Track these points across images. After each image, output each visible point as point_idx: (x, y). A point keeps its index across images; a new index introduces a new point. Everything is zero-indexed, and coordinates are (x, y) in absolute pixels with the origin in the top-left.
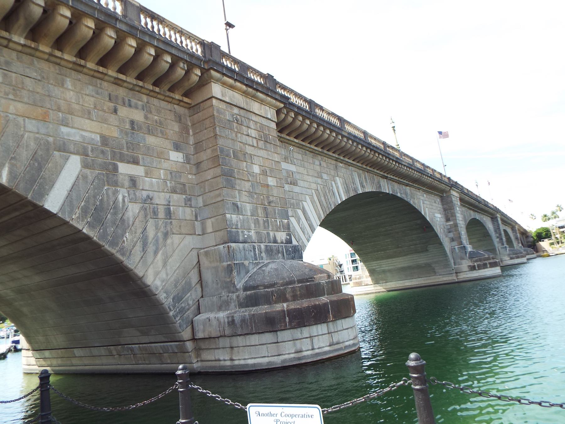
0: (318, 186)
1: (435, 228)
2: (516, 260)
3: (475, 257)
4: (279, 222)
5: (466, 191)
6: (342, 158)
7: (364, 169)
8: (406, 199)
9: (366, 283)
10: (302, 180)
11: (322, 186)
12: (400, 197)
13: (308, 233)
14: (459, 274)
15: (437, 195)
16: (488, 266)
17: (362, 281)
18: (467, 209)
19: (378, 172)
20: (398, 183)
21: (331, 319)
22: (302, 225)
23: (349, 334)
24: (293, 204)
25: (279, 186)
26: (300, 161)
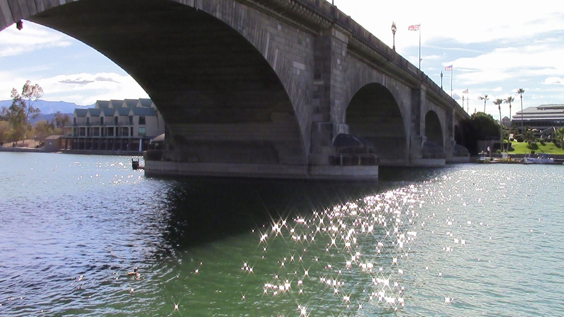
1: (285, 85)
8: (233, 25)
12: (221, 18)
15: (307, 31)
18: (365, 65)
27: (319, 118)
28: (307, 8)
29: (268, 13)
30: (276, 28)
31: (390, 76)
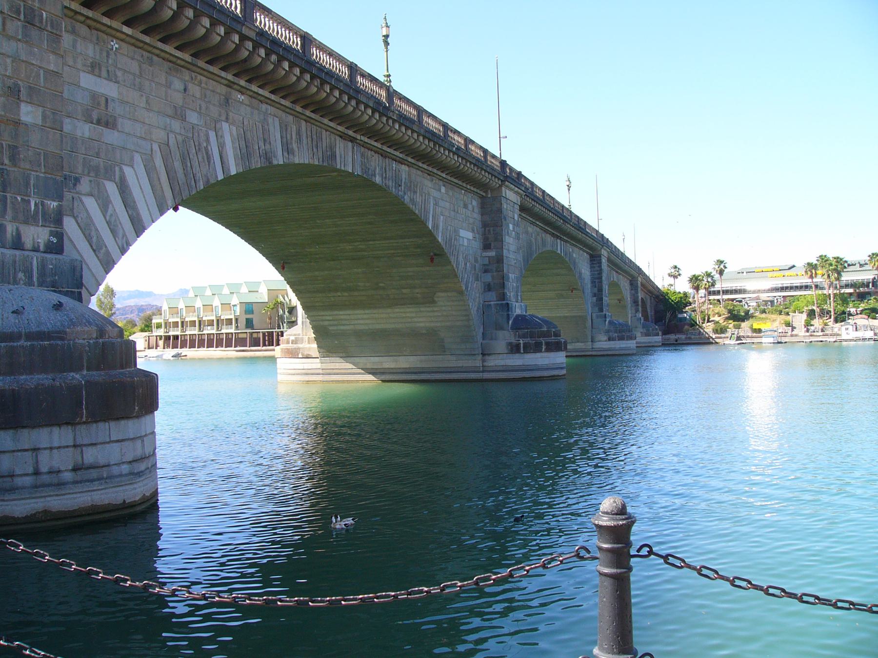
0: (171, 136)
1: (452, 259)
2: (617, 342)
3: (524, 329)
4: (36, 205)
5: (539, 194)
6: (243, 83)
7: (298, 115)
9: (306, 353)
10: (130, 119)
11: (180, 138)
13: (124, 235)
14: (487, 357)
16: (544, 347)
17: (299, 348)
18: (538, 229)
19: (332, 124)
20: (382, 156)
21: (84, 419)
22: (111, 215)
23: (123, 451)
24: (96, 170)
25: (47, 125)
26: (131, 77)
27: (492, 296)
28: (475, 165)
29: (430, 174)
30: (440, 190)
31: (566, 241)
